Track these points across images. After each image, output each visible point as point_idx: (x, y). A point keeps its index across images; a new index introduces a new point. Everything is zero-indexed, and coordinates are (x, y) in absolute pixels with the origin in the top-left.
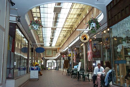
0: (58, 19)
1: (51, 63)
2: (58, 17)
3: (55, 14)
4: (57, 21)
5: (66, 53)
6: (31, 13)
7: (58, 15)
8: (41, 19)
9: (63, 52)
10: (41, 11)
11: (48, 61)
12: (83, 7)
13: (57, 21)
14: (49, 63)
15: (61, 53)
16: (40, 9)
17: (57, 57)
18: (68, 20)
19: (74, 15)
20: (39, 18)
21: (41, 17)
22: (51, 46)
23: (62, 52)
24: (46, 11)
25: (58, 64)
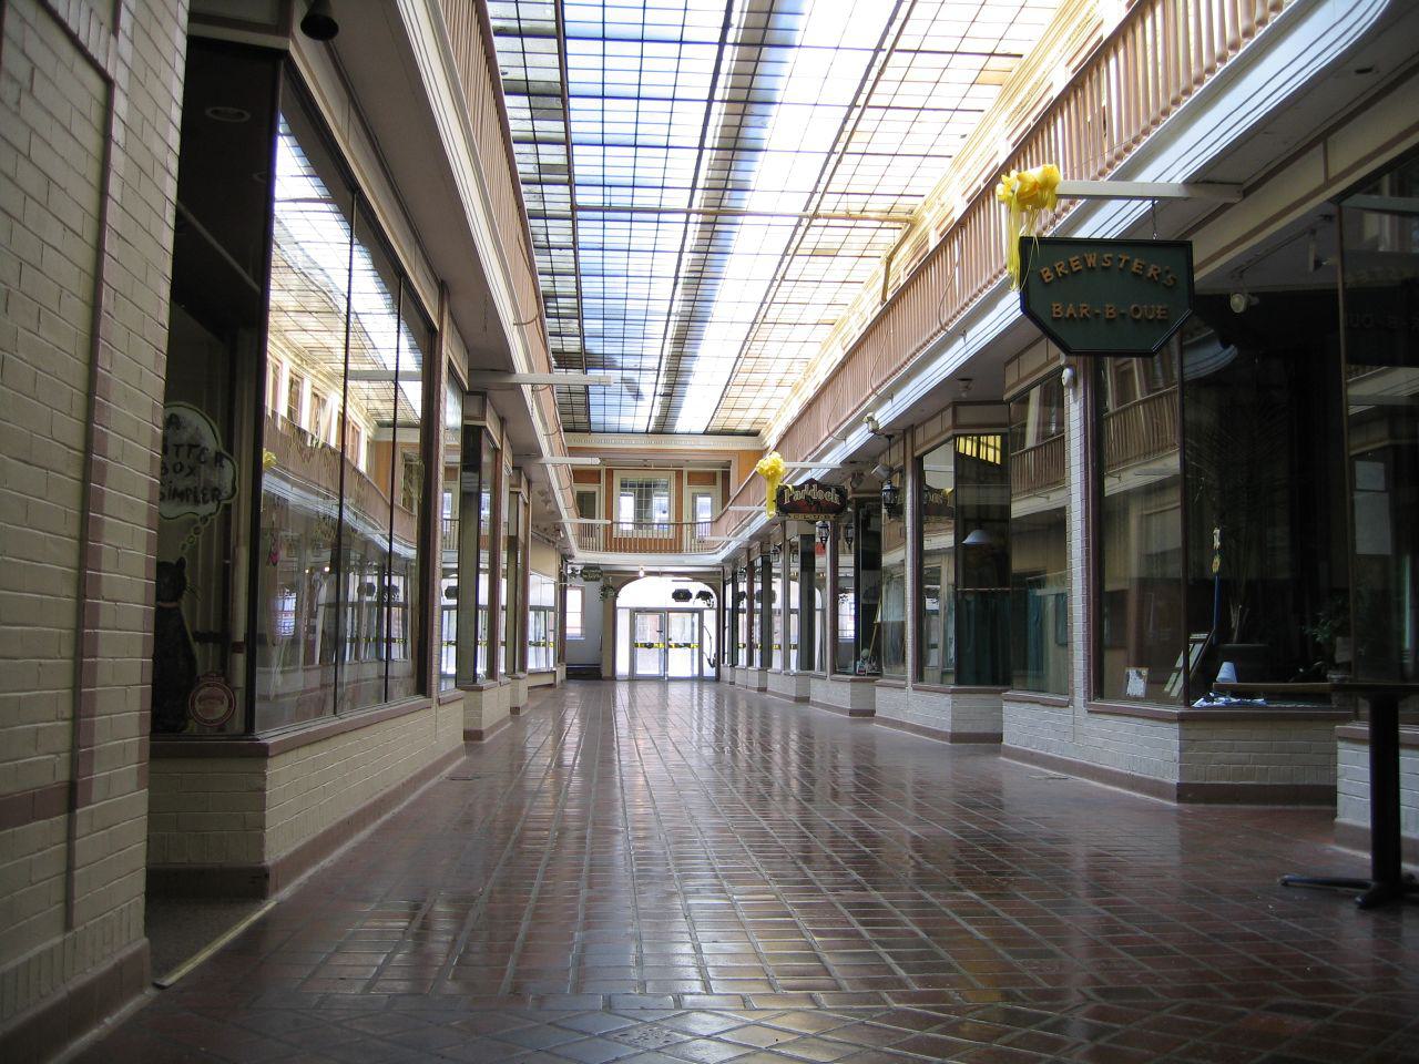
0: (756, 109)
1: (663, 613)
2: (759, 82)
3: (680, 287)
4: (751, 133)
5: (833, 498)
6: (499, 147)
7: (762, 68)
8: (573, 115)
9: (811, 482)
10: (572, 75)
11: (628, 597)
12: (753, 394)
13: (751, 133)
14: (635, 612)
15: (781, 492)
16: (562, 54)
17: (723, 554)
18: (765, 331)
19: (966, 46)
20: (540, 102)
21: (573, 88)
22: (663, 428)
23: (799, 482)
24: (622, 77)
25: (735, 621)
